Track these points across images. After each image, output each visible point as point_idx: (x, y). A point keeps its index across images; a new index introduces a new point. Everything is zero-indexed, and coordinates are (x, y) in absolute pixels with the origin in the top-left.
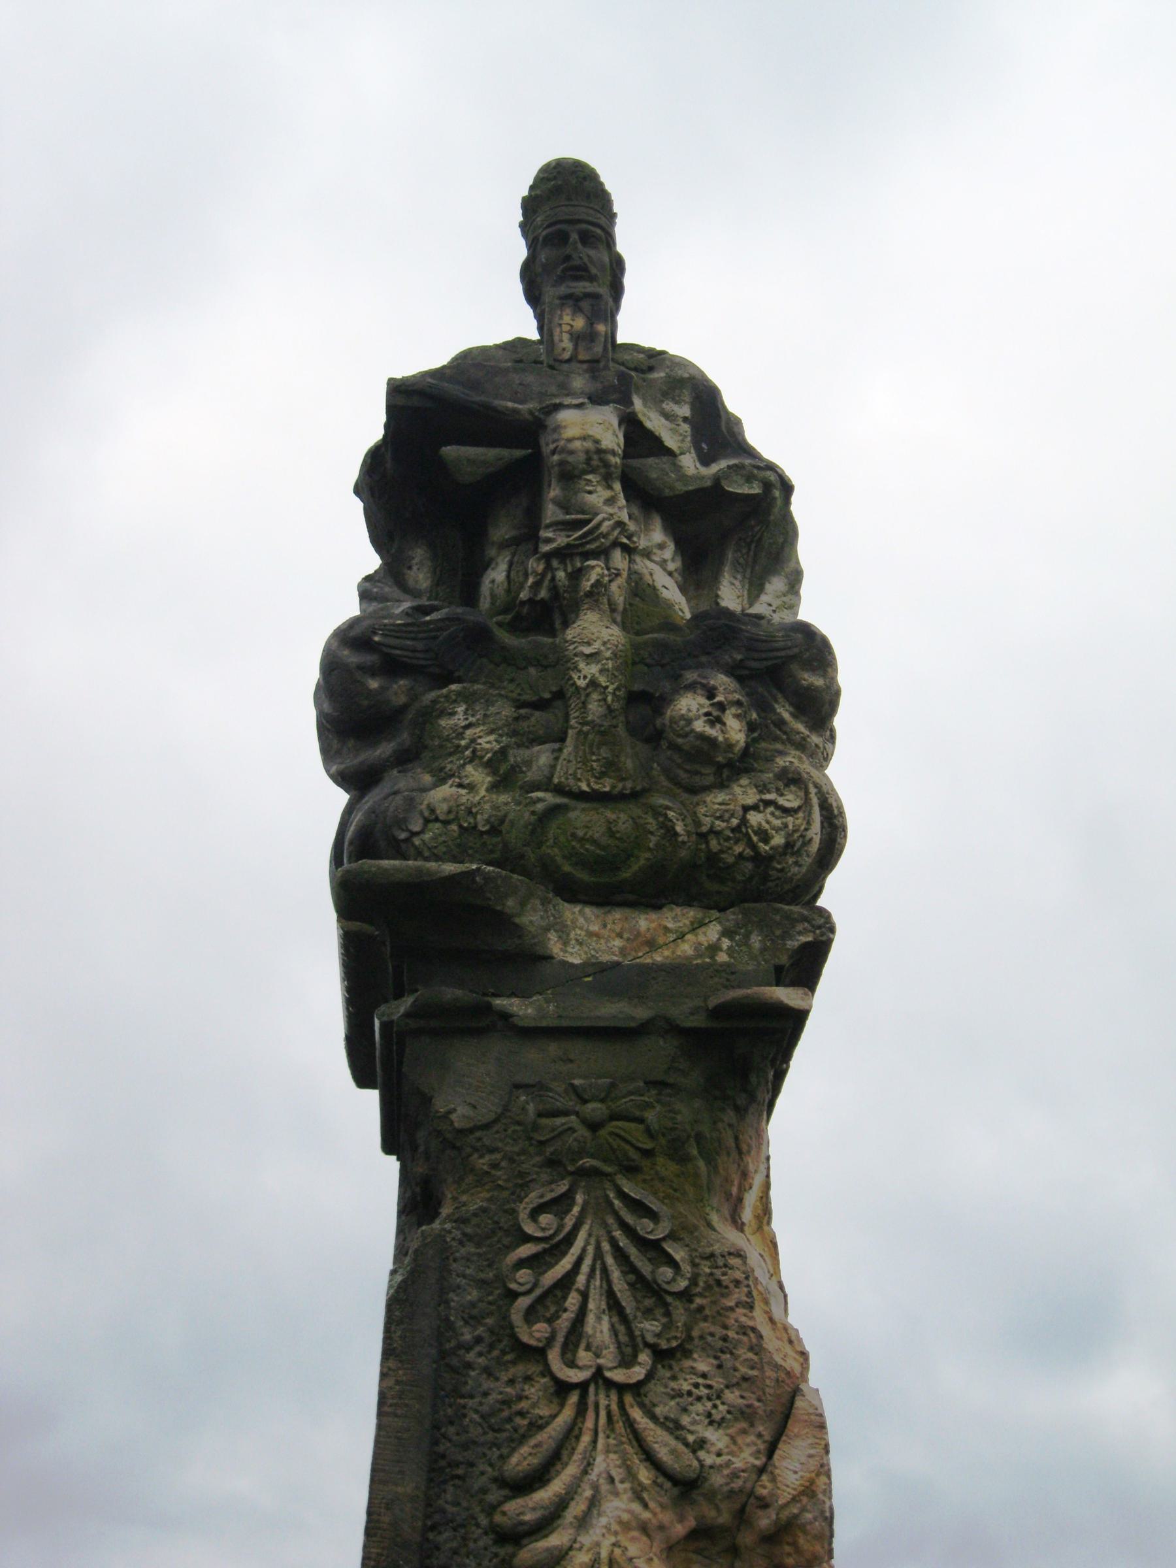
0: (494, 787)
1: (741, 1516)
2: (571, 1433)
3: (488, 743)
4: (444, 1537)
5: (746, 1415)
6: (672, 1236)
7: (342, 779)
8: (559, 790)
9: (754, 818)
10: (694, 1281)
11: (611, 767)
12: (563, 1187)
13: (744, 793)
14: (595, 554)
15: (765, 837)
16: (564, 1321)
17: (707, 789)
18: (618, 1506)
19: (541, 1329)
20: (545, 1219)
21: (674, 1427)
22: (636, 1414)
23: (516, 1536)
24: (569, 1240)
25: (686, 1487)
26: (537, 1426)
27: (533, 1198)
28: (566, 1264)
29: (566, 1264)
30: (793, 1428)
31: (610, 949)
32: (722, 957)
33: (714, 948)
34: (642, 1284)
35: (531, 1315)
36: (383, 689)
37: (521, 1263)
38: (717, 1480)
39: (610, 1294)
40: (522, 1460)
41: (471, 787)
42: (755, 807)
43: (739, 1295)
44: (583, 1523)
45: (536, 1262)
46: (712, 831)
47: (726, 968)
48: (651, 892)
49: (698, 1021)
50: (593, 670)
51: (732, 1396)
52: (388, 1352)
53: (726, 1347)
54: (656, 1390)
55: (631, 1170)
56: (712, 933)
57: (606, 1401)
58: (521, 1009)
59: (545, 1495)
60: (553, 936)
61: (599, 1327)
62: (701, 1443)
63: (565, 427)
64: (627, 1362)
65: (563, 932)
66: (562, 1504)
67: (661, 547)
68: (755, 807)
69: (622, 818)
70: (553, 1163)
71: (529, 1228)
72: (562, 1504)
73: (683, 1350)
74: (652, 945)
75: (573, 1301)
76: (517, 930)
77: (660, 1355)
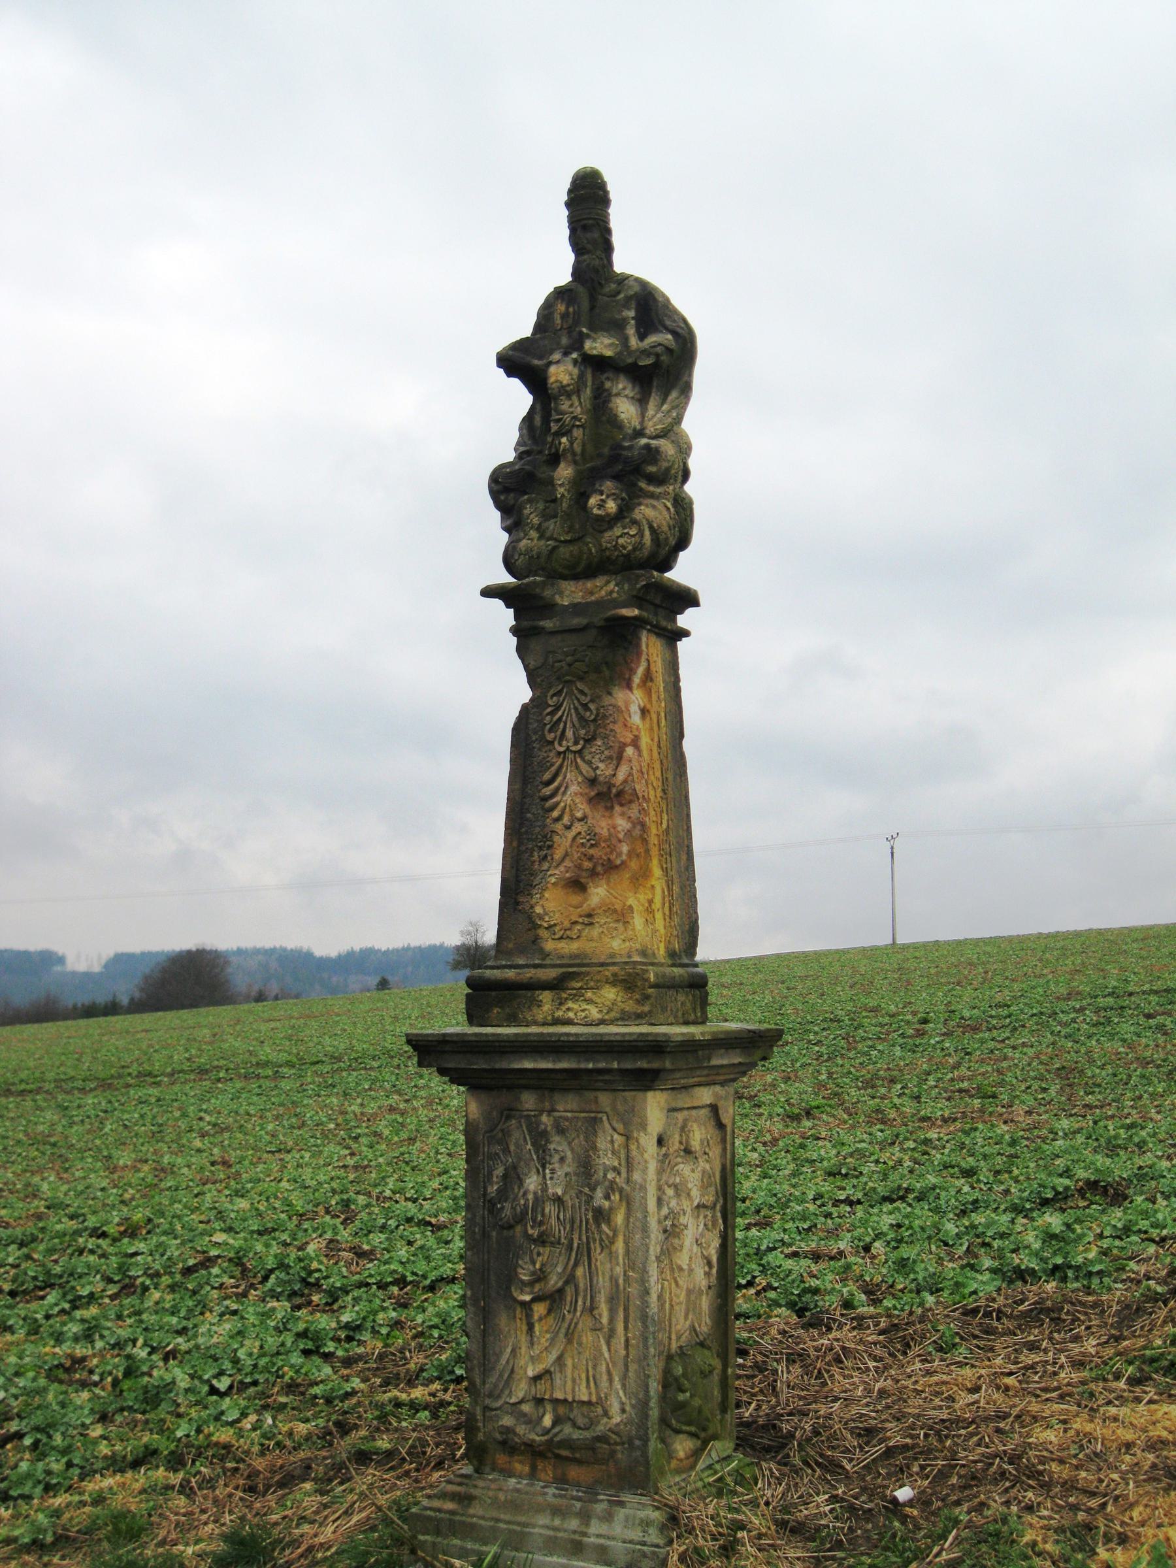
0: (540, 538)
1: (609, 788)
2: (561, 767)
3: (536, 521)
4: (527, 800)
5: (610, 758)
6: (592, 701)
7: (507, 529)
8: (556, 540)
9: (621, 541)
10: (597, 715)
11: (571, 529)
12: (560, 687)
13: (618, 531)
14: (563, 435)
15: (624, 547)
16: (559, 733)
17: (605, 531)
18: (574, 788)
19: (553, 735)
20: (555, 698)
21: (589, 763)
22: (579, 760)
23: (545, 799)
24: (562, 705)
25: (593, 782)
26: (552, 765)
27: (552, 692)
28: (560, 713)
29: (560, 713)
30: (623, 762)
31: (578, 597)
32: (615, 595)
33: (612, 592)
34: (581, 718)
35: (550, 731)
36: (506, 498)
37: (548, 714)
38: (601, 779)
39: (572, 722)
40: (547, 776)
41: (532, 539)
42: (621, 536)
43: (611, 719)
44: (564, 793)
45: (552, 713)
46: (606, 548)
47: (614, 600)
48: (590, 572)
49: (602, 623)
50: (562, 490)
51: (606, 752)
52: (513, 746)
53: (606, 737)
54: (586, 752)
55: (581, 679)
56: (612, 585)
57: (571, 756)
58: (548, 624)
59: (556, 784)
60: (557, 597)
61: (569, 733)
62: (597, 768)
63: (115, 996)
64: (576, 743)
65: (561, 594)
66: (558, 789)
67: (624, 389)
68: (621, 536)
69: (574, 548)
70: (558, 678)
71: (550, 702)
72: (558, 789)
73: (594, 738)
74: (592, 593)
75: (562, 725)
76: (542, 598)
77: (587, 741)
